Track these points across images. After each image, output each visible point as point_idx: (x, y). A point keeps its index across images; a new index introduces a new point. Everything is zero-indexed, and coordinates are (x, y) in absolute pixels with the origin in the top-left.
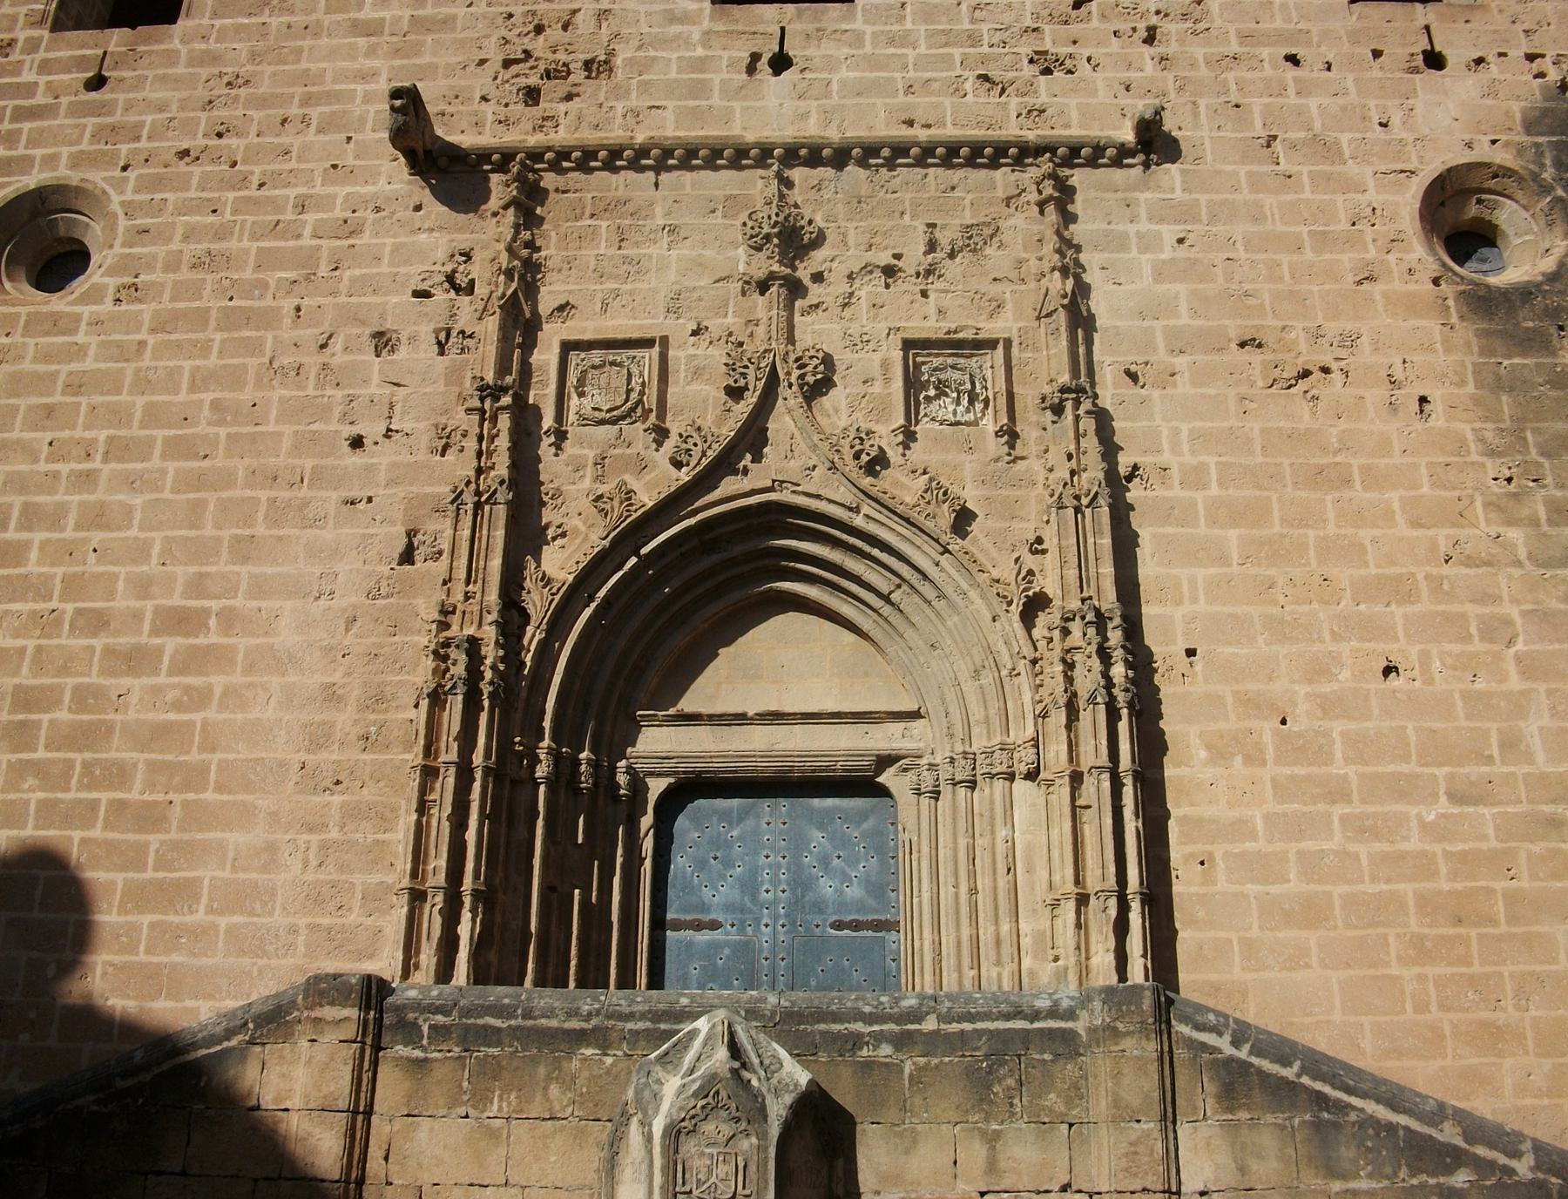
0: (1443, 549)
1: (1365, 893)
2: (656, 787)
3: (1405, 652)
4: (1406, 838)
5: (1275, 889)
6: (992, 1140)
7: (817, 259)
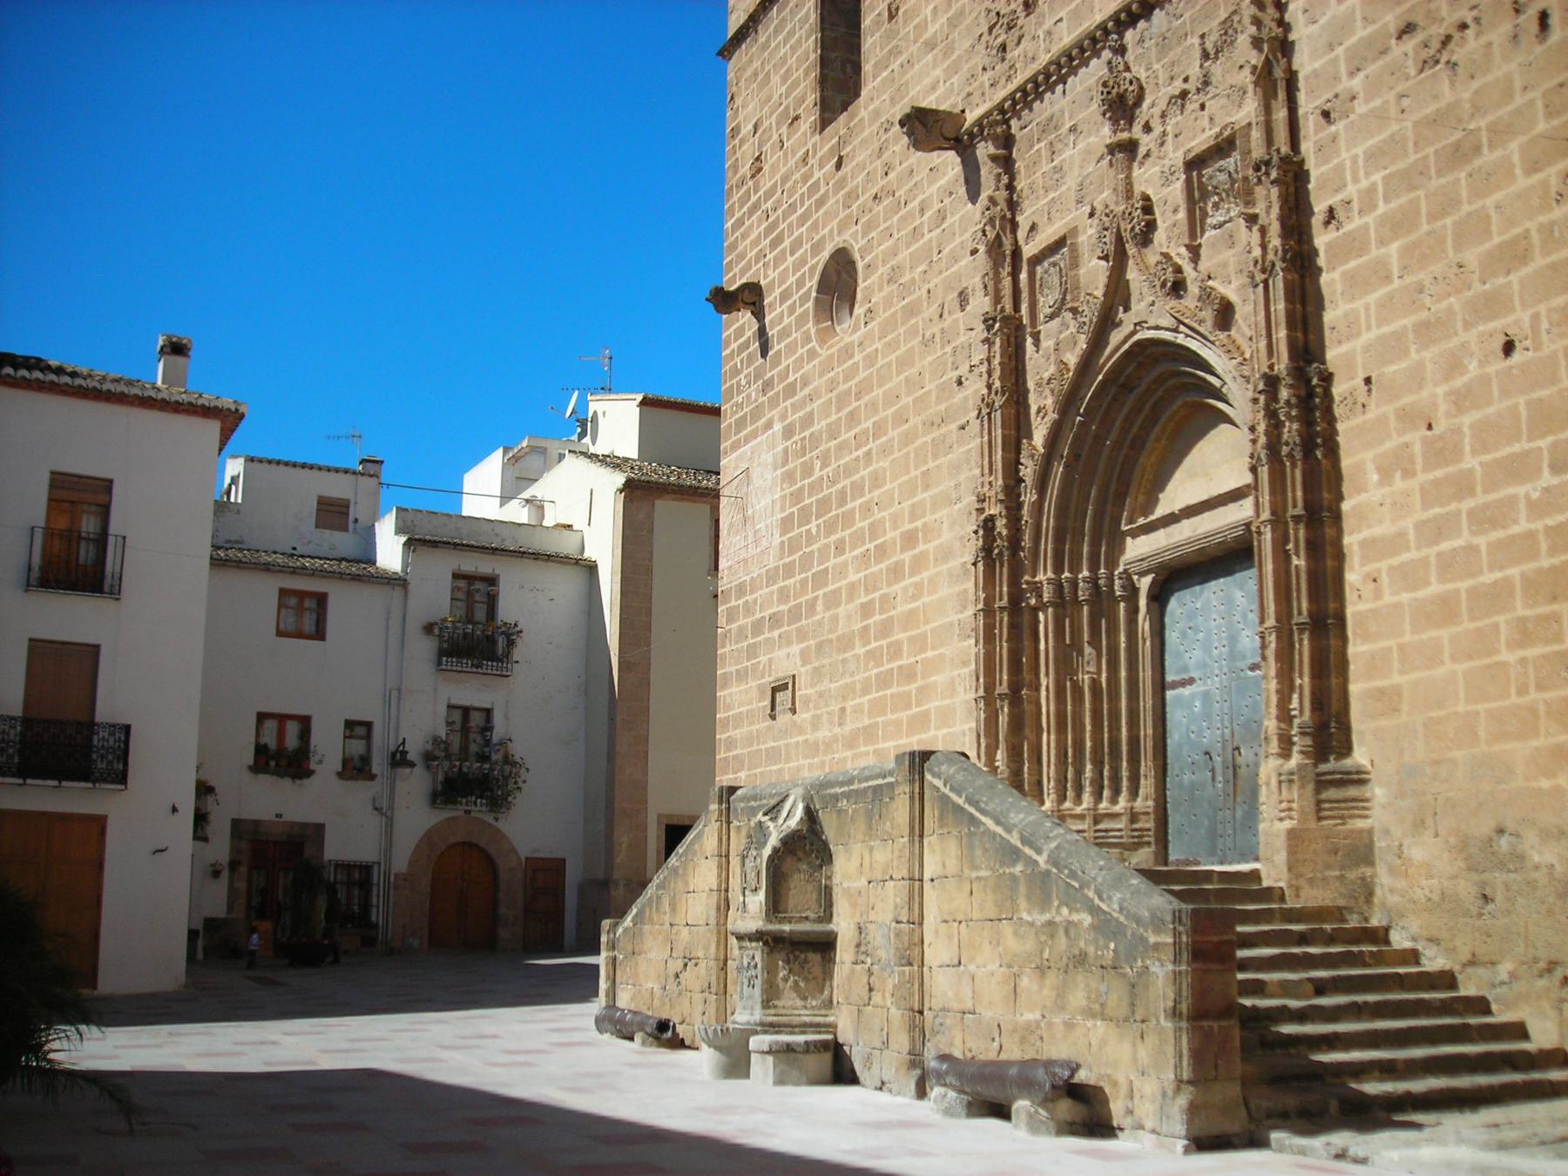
0: (1554, 189)
1: (1484, 584)
2: (1144, 583)
3: (1516, 320)
4: (1516, 522)
5: (1421, 594)
6: (871, 849)
7: (1145, 112)
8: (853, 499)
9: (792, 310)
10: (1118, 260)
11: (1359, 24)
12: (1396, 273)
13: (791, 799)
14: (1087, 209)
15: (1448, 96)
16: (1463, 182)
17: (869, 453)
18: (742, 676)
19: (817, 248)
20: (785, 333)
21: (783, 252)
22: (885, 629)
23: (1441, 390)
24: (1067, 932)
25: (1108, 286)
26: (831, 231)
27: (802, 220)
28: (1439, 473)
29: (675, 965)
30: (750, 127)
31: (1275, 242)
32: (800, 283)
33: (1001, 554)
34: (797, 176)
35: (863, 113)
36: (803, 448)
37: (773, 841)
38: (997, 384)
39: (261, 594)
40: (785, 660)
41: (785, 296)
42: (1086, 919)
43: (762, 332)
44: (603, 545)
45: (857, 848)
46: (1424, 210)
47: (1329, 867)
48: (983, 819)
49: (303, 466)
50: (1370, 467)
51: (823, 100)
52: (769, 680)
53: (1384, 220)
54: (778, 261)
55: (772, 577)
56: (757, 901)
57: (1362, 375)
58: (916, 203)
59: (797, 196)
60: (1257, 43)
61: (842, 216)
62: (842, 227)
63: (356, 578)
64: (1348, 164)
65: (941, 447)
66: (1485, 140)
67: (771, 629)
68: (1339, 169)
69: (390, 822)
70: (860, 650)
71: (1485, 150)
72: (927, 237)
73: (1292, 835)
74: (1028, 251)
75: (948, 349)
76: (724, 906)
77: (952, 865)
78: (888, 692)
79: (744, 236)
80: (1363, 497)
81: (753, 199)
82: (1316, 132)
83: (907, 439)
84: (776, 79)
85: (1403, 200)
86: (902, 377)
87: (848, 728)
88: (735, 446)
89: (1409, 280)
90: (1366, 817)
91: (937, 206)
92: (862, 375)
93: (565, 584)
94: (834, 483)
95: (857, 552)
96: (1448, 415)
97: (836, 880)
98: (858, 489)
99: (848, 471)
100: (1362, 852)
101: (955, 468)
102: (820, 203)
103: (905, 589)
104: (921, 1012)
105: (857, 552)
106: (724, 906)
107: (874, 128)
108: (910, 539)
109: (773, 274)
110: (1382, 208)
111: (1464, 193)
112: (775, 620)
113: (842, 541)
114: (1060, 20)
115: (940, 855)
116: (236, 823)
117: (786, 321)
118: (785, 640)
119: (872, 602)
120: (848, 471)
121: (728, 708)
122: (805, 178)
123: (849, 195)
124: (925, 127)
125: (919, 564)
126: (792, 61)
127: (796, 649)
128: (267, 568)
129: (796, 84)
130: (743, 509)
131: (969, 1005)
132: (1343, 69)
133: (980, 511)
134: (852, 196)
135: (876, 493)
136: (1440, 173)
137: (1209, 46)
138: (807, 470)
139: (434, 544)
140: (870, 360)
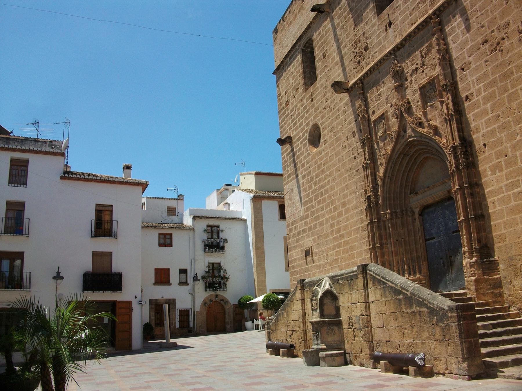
6: (351, 294)
8: (325, 194)
9: (301, 143)
10: (401, 117)
11: (470, 42)
12: (490, 113)
13: (324, 281)
14: (390, 105)
15: (500, 59)
16: (509, 84)
17: (329, 181)
18: (295, 248)
19: (307, 125)
20: (300, 149)
21: (297, 126)
22: (339, 230)
23: (509, 145)
24: (419, 315)
25: (399, 126)
26: (311, 119)
27: (302, 117)
28: (511, 169)
29: (289, 333)
30: (284, 93)
31: (451, 107)
32: (303, 135)
33: (373, 206)
34: (300, 105)
35: (318, 85)
36: (309, 181)
37: (320, 294)
38: (367, 158)
39: (154, 236)
40: (308, 242)
41: (299, 139)
42: (426, 310)
43: (292, 150)
44: (247, 214)
45: (346, 295)
46: (497, 93)
47: (489, 289)
48: (387, 282)
49: (163, 198)
50: (488, 170)
51: (305, 83)
52: (305, 248)
53: (484, 98)
54: (296, 129)
55: (302, 219)
56: (317, 313)
57: (482, 143)
58: (336, 109)
59: (300, 111)
60: (439, 51)
61: (314, 114)
62: (315, 117)
63: (180, 228)
64: (471, 82)
65: (351, 177)
66: (514, 71)
67: (303, 233)
68: (468, 84)
69: (194, 298)
70: (331, 237)
71: (515, 73)
72: (341, 118)
73: (476, 281)
74: (373, 118)
75: (351, 149)
76: (304, 314)
77: (379, 297)
78: (341, 249)
79: (285, 123)
80: (487, 178)
81: (287, 113)
82: (460, 74)
83: (340, 176)
84: (290, 79)
85: (490, 90)
86: (337, 158)
87: (329, 261)
88: (287, 183)
89: (494, 114)
90: (499, 274)
91: (343, 109)
92: (325, 159)
93: (238, 226)
94: (319, 191)
95: (327, 210)
96: (511, 152)
97: (341, 304)
98: (326, 191)
99: (323, 187)
100: (498, 284)
101: (356, 183)
102: (307, 112)
103: (344, 219)
104: (372, 342)
105: (327, 210)
106: (304, 314)
107: (322, 89)
108: (344, 204)
109: (294, 133)
110: (483, 94)
111: (509, 87)
112: (304, 231)
113: (323, 206)
114: (376, 52)
115: (374, 294)
116: (151, 300)
117: (300, 146)
118: (308, 236)
119: (333, 223)
120: (323, 187)
121: (292, 257)
122: (302, 105)
123: (316, 109)
124: (338, 87)
125: (347, 211)
126: (295, 73)
127: (311, 238)
128: (155, 227)
129: (297, 79)
130: (291, 200)
131: (388, 339)
132: (466, 56)
133: (365, 195)
134: (317, 109)
135: (332, 192)
136: (501, 82)
137: (423, 54)
138: (310, 187)
139: (201, 217)
140: (327, 154)
